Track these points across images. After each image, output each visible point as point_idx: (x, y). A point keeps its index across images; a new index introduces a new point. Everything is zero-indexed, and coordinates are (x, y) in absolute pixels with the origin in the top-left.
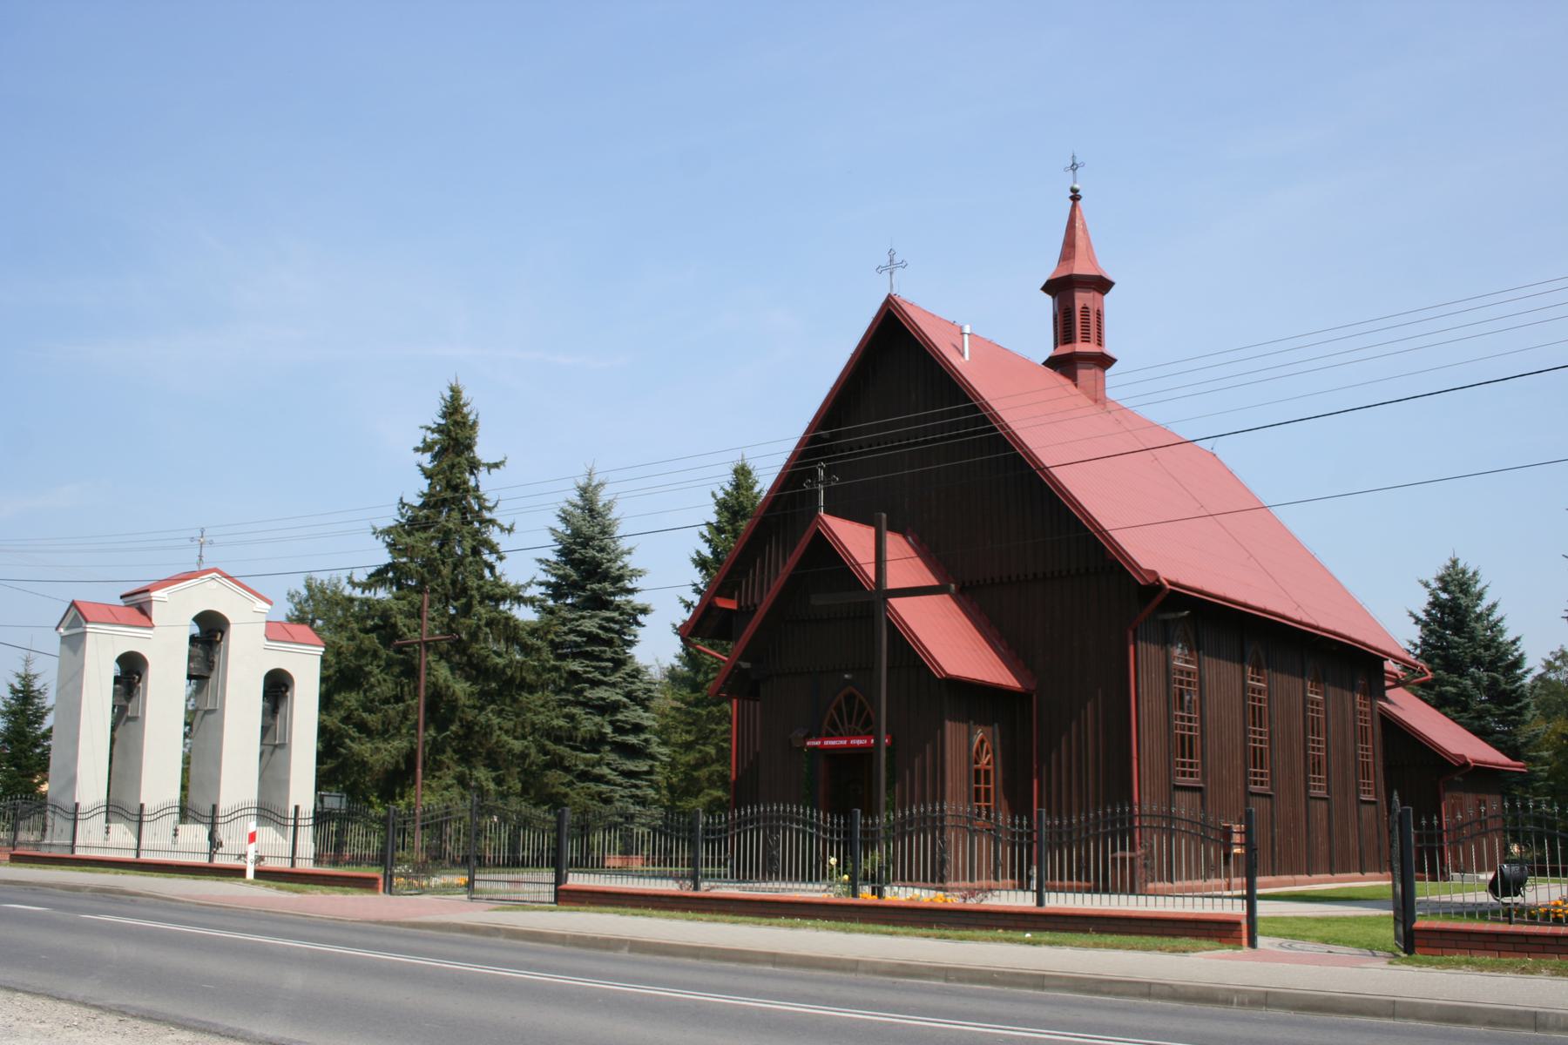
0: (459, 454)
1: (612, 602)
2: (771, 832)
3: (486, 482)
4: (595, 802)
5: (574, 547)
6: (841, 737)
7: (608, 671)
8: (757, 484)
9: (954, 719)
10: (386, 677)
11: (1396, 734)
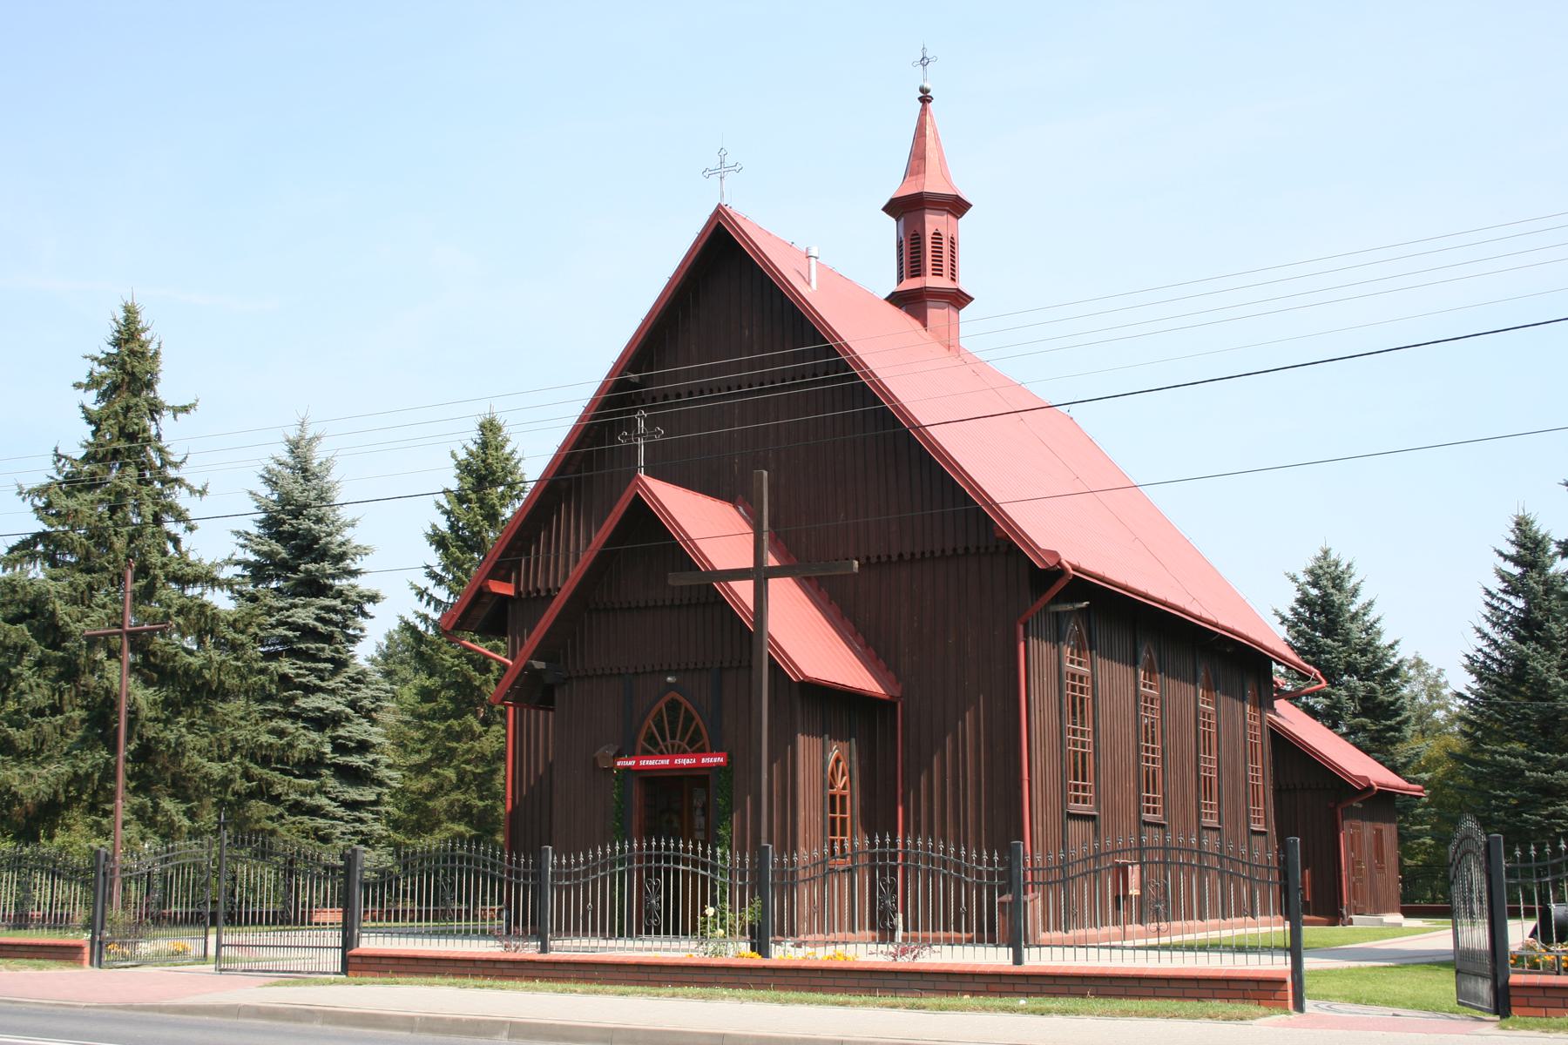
0: (136, 394)
1: (331, 587)
2: (649, 875)
3: (170, 432)
4: (310, 841)
5: (283, 516)
6: (662, 754)
7: (327, 674)
8: (509, 444)
9: (808, 733)
10: (41, 681)
11: (1284, 747)
